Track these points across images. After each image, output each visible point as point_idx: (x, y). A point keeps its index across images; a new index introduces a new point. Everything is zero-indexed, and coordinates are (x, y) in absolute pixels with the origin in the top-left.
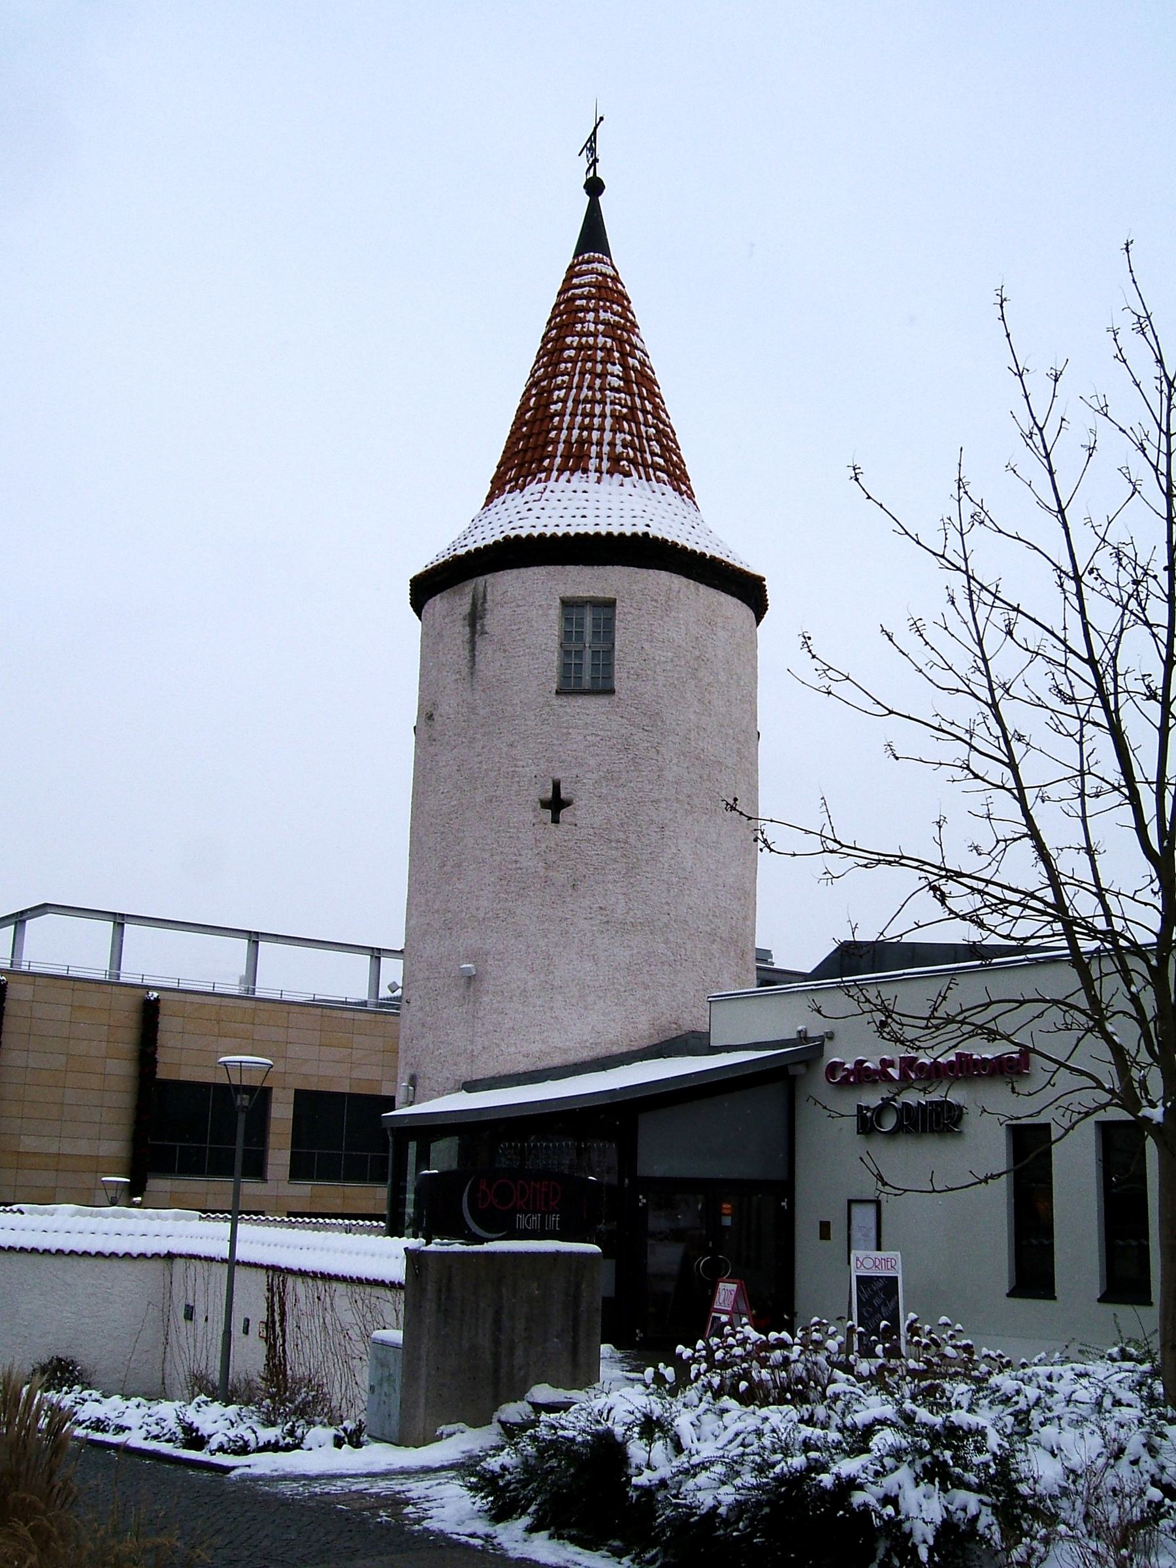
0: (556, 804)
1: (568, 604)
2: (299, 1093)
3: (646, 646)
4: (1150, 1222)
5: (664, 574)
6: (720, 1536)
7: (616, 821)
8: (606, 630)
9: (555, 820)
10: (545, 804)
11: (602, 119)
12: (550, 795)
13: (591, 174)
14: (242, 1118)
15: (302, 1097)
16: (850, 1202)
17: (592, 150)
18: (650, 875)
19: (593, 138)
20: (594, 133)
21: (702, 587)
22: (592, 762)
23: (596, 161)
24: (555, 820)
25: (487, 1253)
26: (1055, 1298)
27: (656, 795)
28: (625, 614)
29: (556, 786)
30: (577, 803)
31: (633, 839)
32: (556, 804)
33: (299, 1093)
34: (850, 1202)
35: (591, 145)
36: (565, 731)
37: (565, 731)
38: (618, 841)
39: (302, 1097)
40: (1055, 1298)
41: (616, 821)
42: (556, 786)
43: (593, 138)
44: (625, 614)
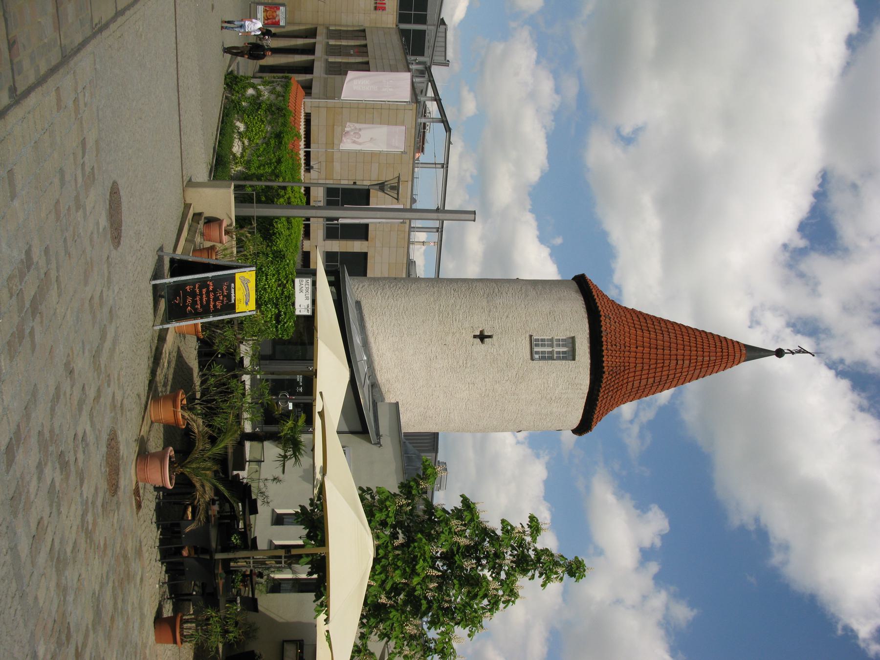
1: (572, 342)
2: (366, 254)
3: (554, 375)
4: (588, 356)
5: (588, 382)
6: (253, 380)
7: (475, 362)
9: (475, 337)
10: (482, 332)
12: (486, 334)
15: (365, 255)
16: (284, 641)
17: (799, 352)
19: (805, 352)
21: (585, 400)
22: (501, 352)
23: (793, 353)
24: (475, 337)
25: (174, 378)
27: (487, 380)
29: (490, 337)
30: (483, 346)
31: (468, 370)
32: (482, 337)
33: (366, 254)
39: (365, 255)
41: (475, 362)
42: (490, 337)
43: (805, 352)
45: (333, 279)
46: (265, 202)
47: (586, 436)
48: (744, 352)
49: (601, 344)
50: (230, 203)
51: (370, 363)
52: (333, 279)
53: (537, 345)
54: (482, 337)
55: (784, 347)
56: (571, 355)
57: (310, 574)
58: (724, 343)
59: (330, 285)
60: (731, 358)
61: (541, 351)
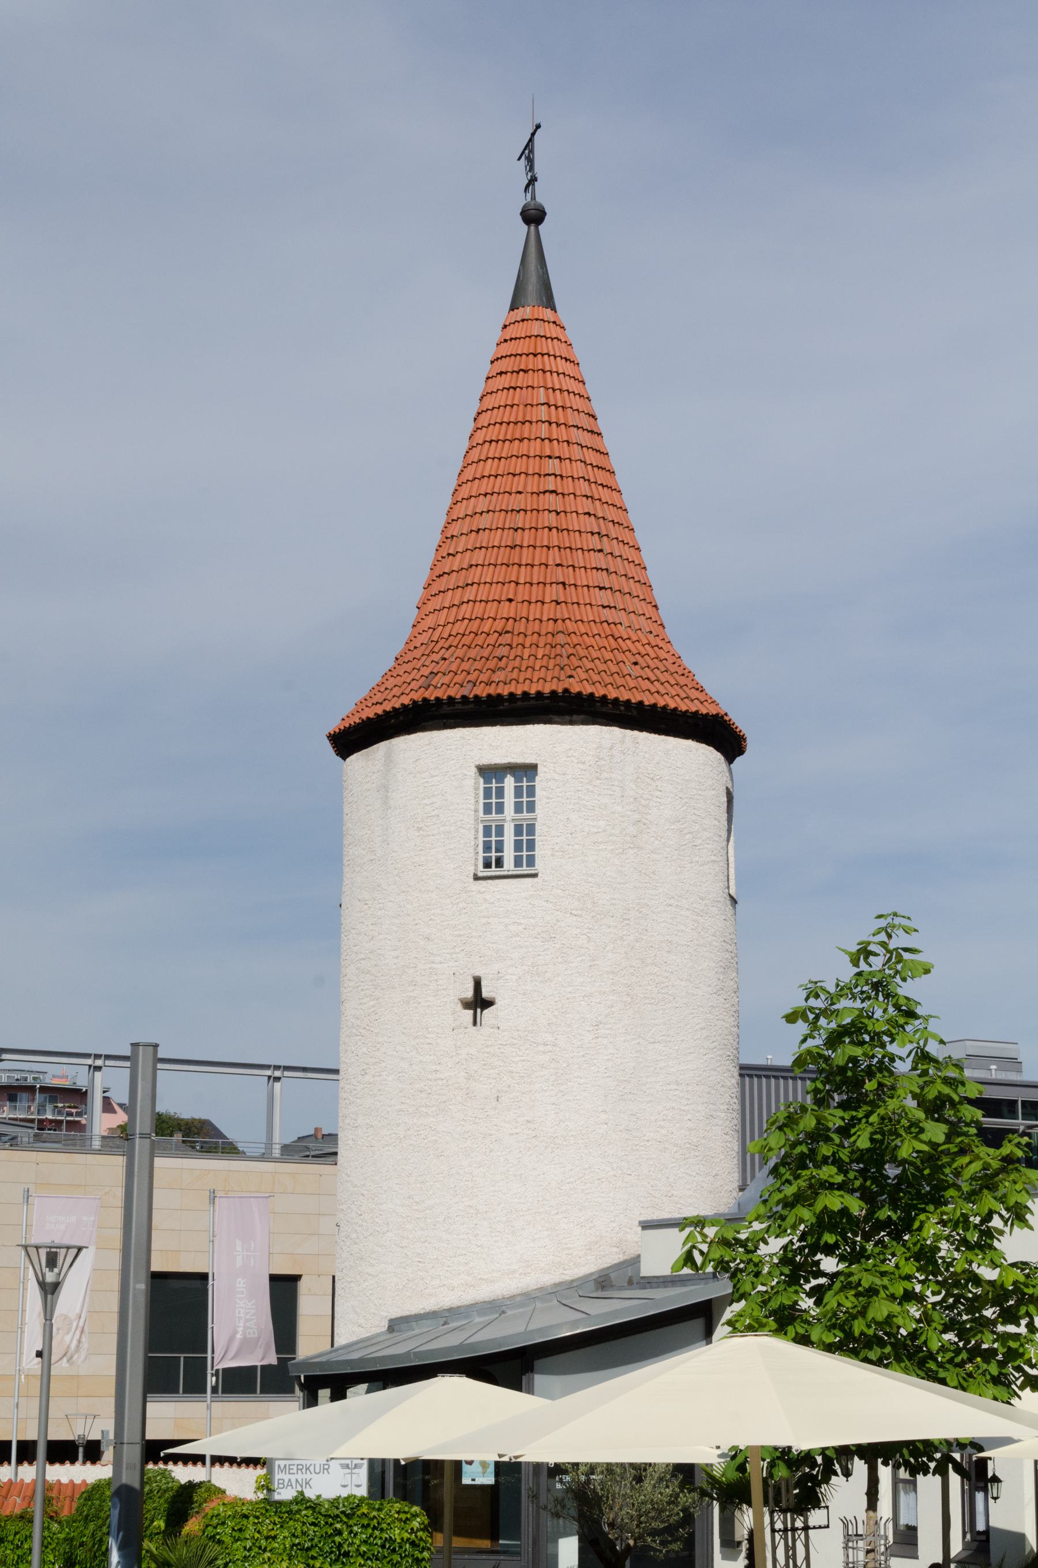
0: (479, 1002)
1: (490, 772)
8: (526, 802)
10: (466, 1005)
11: (538, 127)
12: (469, 994)
13: (530, 174)
14: (81, 1450)
16: (828, 1527)
17: (530, 161)
18: (582, 1081)
19: (530, 145)
20: (531, 140)
23: (533, 181)
26: (917, 1558)
28: (548, 780)
34: (828, 1527)
35: (528, 153)
36: (484, 921)
37: (484, 921)
38: (545, 1044)
40: (917, 1558)
43: (530, 145)
44: (548, 780)
45: (324, 1393)
46: (43, 1543)
47: (740, 721)
48: (526, 312)
49: (495, 700)
50: (132, 1348)
51: (528, 1298)
52: (324, 1393)
53: (499, 863)
54: (479, 1002)
55: (521, 200)
56: (526, 771)
57: (836, 1474)
58: (455, 529)
59: (343, 1396)
60: (543, 346)
61: (506, 854)
